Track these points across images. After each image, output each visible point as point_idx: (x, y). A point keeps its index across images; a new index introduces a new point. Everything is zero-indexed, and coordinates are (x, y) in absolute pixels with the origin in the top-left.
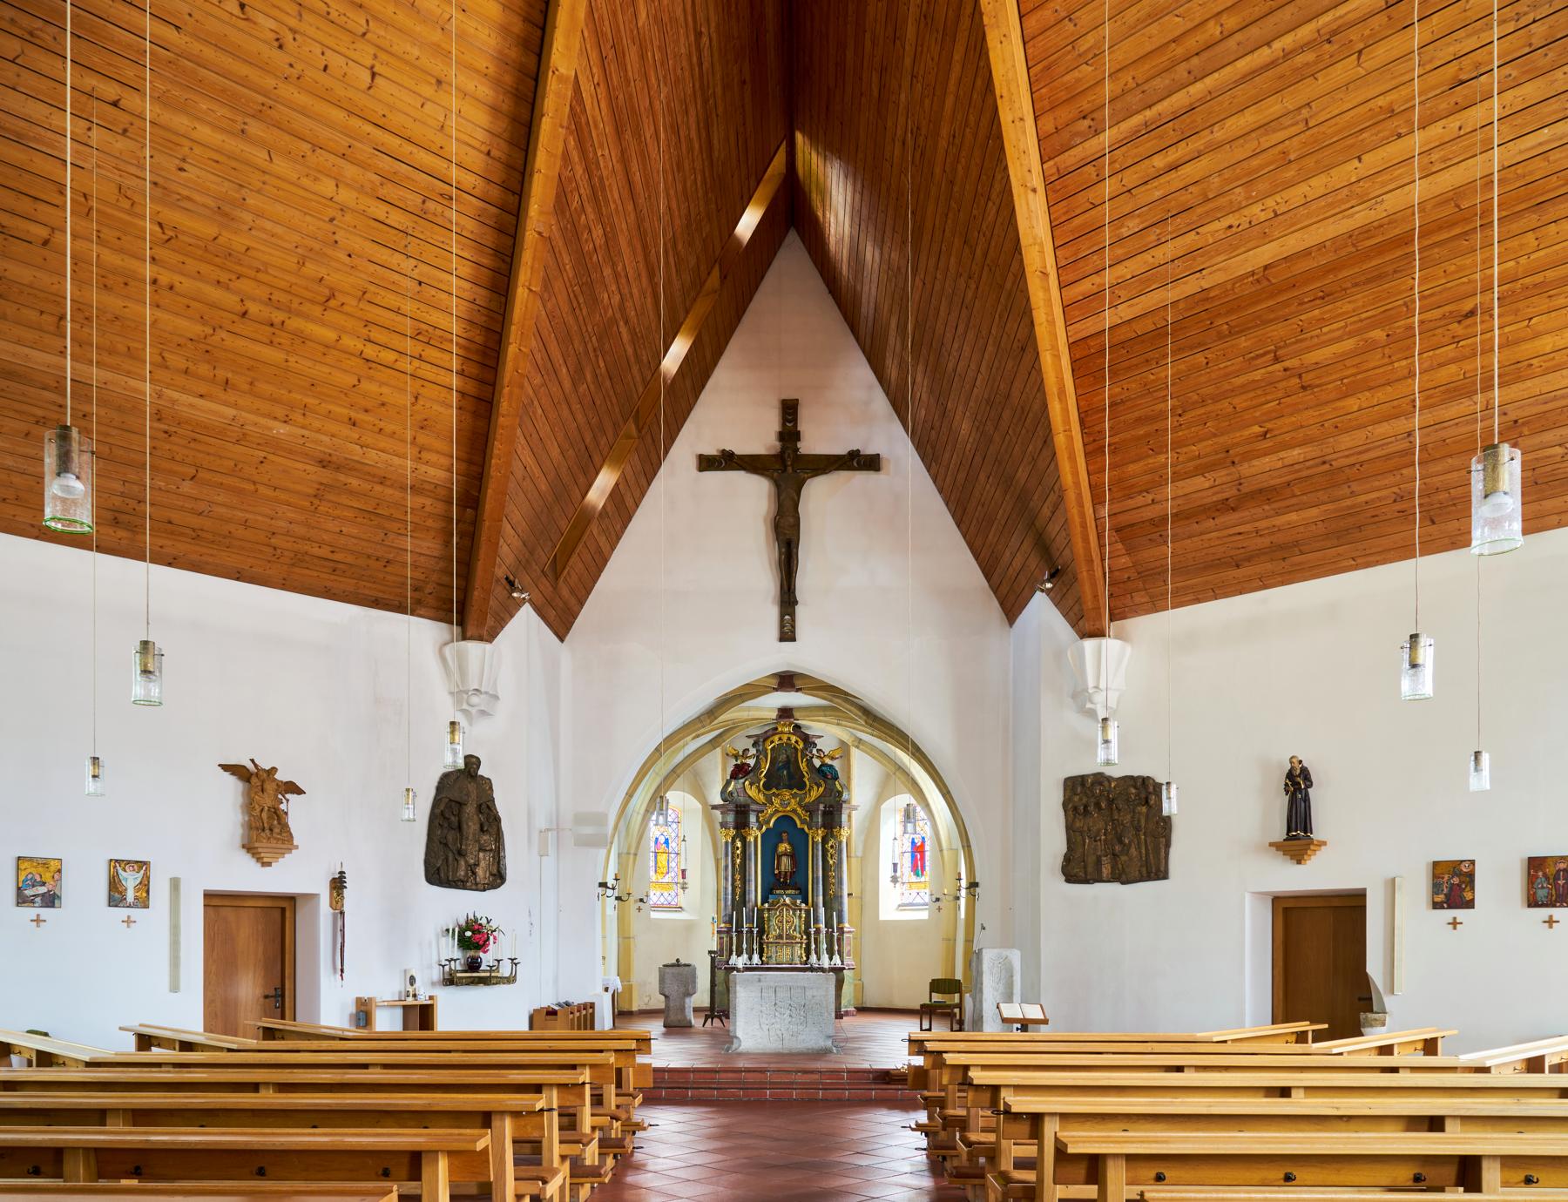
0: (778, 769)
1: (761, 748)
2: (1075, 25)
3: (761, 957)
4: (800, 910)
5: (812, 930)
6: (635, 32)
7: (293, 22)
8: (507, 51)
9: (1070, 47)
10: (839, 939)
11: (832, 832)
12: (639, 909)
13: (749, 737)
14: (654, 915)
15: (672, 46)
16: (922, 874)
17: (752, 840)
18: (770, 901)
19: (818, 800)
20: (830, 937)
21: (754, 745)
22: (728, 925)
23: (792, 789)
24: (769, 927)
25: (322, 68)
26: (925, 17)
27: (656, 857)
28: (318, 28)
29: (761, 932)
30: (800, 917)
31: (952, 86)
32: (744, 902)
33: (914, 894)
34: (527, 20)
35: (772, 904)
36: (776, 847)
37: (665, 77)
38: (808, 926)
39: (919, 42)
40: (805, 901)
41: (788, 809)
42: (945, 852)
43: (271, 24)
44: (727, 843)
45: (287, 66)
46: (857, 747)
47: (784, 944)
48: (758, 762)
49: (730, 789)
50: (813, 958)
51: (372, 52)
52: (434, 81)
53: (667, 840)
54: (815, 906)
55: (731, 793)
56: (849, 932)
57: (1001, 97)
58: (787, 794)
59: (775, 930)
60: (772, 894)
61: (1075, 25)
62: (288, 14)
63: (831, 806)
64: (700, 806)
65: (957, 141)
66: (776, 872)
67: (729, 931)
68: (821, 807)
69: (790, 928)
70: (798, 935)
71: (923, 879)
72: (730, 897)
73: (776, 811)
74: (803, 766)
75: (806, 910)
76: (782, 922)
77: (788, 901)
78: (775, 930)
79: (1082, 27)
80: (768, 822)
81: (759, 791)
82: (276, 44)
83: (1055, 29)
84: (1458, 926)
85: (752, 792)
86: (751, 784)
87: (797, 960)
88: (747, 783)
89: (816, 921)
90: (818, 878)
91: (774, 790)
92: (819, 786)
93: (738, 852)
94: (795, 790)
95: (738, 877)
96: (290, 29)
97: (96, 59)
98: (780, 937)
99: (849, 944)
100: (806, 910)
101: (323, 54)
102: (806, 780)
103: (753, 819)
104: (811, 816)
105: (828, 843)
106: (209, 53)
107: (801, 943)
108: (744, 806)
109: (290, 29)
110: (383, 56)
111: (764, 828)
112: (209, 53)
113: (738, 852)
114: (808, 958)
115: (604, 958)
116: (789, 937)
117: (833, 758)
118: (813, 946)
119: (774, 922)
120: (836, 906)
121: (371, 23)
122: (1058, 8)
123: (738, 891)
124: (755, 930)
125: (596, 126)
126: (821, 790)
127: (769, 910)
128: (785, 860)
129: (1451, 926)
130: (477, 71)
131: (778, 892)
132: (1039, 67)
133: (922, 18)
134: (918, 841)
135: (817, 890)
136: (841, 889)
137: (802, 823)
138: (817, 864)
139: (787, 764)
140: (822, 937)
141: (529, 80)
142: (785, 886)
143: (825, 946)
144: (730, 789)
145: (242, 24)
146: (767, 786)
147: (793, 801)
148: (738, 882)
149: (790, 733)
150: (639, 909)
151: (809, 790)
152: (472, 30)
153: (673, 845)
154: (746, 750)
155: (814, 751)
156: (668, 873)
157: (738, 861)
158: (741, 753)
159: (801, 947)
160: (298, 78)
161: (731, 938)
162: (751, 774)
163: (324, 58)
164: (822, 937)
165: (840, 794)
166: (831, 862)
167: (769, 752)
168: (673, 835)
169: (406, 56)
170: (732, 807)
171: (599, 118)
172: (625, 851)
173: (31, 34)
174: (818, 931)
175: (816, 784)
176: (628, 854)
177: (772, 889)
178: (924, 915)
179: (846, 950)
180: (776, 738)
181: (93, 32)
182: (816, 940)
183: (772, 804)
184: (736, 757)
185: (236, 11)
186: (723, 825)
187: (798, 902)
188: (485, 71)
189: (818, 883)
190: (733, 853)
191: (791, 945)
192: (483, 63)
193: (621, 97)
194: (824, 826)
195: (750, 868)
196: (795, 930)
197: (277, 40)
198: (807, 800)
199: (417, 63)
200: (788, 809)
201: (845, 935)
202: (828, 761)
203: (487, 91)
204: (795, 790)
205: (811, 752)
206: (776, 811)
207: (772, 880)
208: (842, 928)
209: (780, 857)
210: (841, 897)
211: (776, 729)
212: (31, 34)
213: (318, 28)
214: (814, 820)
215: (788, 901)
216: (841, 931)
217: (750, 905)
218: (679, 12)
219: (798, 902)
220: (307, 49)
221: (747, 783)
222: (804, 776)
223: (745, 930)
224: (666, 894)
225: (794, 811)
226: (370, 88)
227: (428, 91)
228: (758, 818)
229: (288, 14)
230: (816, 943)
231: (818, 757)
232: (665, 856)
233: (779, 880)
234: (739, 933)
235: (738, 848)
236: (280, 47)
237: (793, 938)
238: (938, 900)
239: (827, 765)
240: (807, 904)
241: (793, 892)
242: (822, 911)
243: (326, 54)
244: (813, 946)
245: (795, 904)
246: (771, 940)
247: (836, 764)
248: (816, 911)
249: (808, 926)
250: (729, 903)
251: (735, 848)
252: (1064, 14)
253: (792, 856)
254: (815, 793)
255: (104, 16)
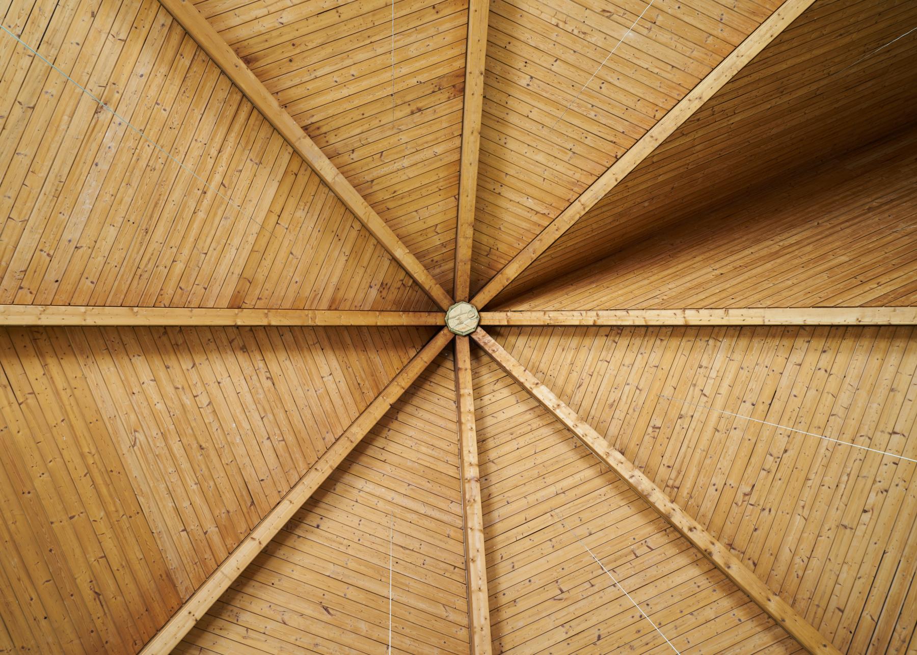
2: (722, 15)
6: (851, 262)
7: (870, 482)
8: (865, 347)
9: (735, 9)
15: (871, 229)
25: (895, 466)
26: (782, 92)
28: (871, 467)
31: (808, 56)
34: (843, 337)
37: (891, 229)
39: (802, 85)
43: (873, 495)
45: (898, 488)
51: (880, 433)
52: (892, 394)
57: (772, 36)
61: (722, 15)
62: (865, 485)
65: (842, 31)
79: (721, 10)
82: (885, 493)
83: (730, 24)
96: (873, 484)
97: (913, 607)
101: (886, 465)
106: (897, 536)
109: (873, 484)
110: (881, 427)
112: (897, 536)
115: (647, 644)
121: (862, 434)
122: (719, 31)
125: (910, 278)
130: (881, 366)
132: (755, 18)
133: (784, 93)
141: (881, 332)
145: (876, 513)
152: (856, 371)
160: (905, 481)
163: (888, 464)
169: (879, 412)
171: (904, 277)
173: (904, 642)
181: (896, 604)
185: (868, 515)
188: (880, 360)
192: (875, 362)
193: (893, 262)
197: (882, 492)
199: (882, 405)
203: (893, 358)
212: (904, 642)
213: (871, 467)
218: (849, 231)
220: (885, 474)
226: (903, 435)
227: (899, 398)
229: (865, 485)
236: (887, 491)
243: (886, 463)
252: (721, 25)
255: (885, 595)
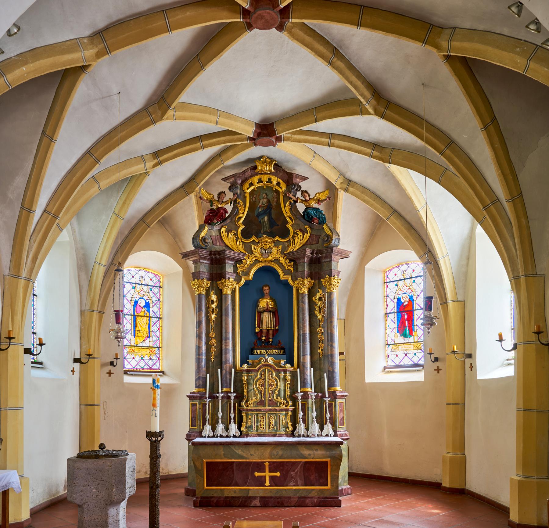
0: (259, 215)
1: (239, 191)
3: (239, 428)
4: (285, 371)
5: (300, 395)
10: (330, 405)
11: (320, 283)
12: (110, 373)
13: (225, 179)
14: (127, 379)
16: (411, 334)
17: (229, 292)
18: (250, 361)
19: (303, 248)
20: (320, 401)
21: (230, 189)
22: (201, 390)
23: (274, 237)
24: (248, 392)
27: (135, 321)
29: (240, 397)
30: (285, 380)
32: (220, 362)
33: (402, 356)
35: (253, 365)
36: (257, 302)
38: (294, 390)
40: (290, 361)
41: (270, 258)
42: (450, 305)
44: (200, 296)
46: (346, 190)
47: (266, 411)
48: (235, 208)
49: (203, 234)
50: (301, 427)
53: (147, 305)
54: (301, 365)
55: (204, 239)
56: (342, 397)
58: (267, 241)
59: (255, 395)
60: (252, 354)
63: (319, 252)
64: (181, 269)
66: (257, 330)
67: (202, 397)
68: (308, 252)
69: (273, 393)
70: (283, 401)
71: (411, 339)
72: (204, 357)
73: (257, 261)
74: (286, 212)
75: (291, 372)
76: (263, 385)
77: (270, 361)
78: (255, 395)
80: (247, 274)
81: (237, 239)
84: (112, 375)
85: (230, 240)
86: (228, 231)
87: (282, 431)
88: (223, 230)
89: (304, 384)
90: (304, 335)
91: (254, 238)
92: (304, 232)
93: (214, 306)
94: (277, 238)
95: (213, 334)
98: (262, 403)
99: (342, 411)
100: (291, 372)
102: (289, 226)
103: (229, 269)
104: (295, 266)
105: (315, 295)
107: (287, 410)
108: (219, 253)
111: (243, 281)
113: (214, 306)
114: (294, 428)
116: (272, 403)
117: (319, 201)
118: (301, 414)
119: (254, 386)
120: (325, 366)
123: (213, 350)
124: (233, 396)
126: (307, 236)
127: (248, 371)
128: (266, 316)
129: (108, 375)
131: (259, 352)
134: (405, 301)
135: (304, 349)
136: (332, 347)
137: (285, 274)
138: (303, 319)
139: (268, 209)
140: (311, 402)
142: (267, 345)
143: (315, 414)
144: (203, 234)
146: (246, 234)
147: (275, 250)
148: (213, 341)
149: (271, 173)
150: (110, 373)
151: (293, 237)
153: (154, 309)
154: (221, 194)
155: (299, 194)
156: (149, 337)
157: (213, 316)
158: (216, 198)
159: (286, 415)
161: (204, 405)
162: (228, 221)
164: (311, 402)
165: (329, 238)
166: (320, 317)
167: (248, 196)
168: (155, 299)
170: (205, 253)
172: (88, 308)
174: (306, 396)
175: (301, 230)
176: (91, 311)
177: (252, 350)
178: (419, 377)
179: (339, 417)
180: (255, 179)
182: (303, 405)
183: (252, 253)
184: (211, 202)
186: (196, 275)
187: (283, 362)
189: (304, 341)
190: (207, 308)
191: (275, 413)
194: (311, 275)
195: (227, 324)
196: (279, 395)
198: (290, 250)
200: (270, 258)
201: (338, 400)
202: (314, 205)
204: (277, 238)
205: (295, 195)
206: (257, 261)
207: (253, 339)
208: (335, 392)
209: (261, 313)
210: (332, 356)
211: (255, 168)
214: (300, 269)
215: (270, 361)
216: (333, 395)
217: (226, 367)
219: (283, 362)
221: (223, 230)
222: (287, 222)
223: (220, 395)
224: (146, 358)
225: (276, 261)
228: (236, 269)
230: (303, 410)
231: (302, 201)
232: (145, 320)
233: (260, 339)
234: (214, 398)
235: (213, 302)
237: (278, 404)
238: (436, 359)
239: (313, 208)
240: (292, 365)
241: (276, 352)
242: (309, 372)
244: (301, 414)
245: (278, 364)
246: (251, 407)
247: (322, 207)
248: (303, 373)
249: (294, 390)
250: (203, 364)
251: (209, 302)
253: (274, 312)
254: (299, 242)
